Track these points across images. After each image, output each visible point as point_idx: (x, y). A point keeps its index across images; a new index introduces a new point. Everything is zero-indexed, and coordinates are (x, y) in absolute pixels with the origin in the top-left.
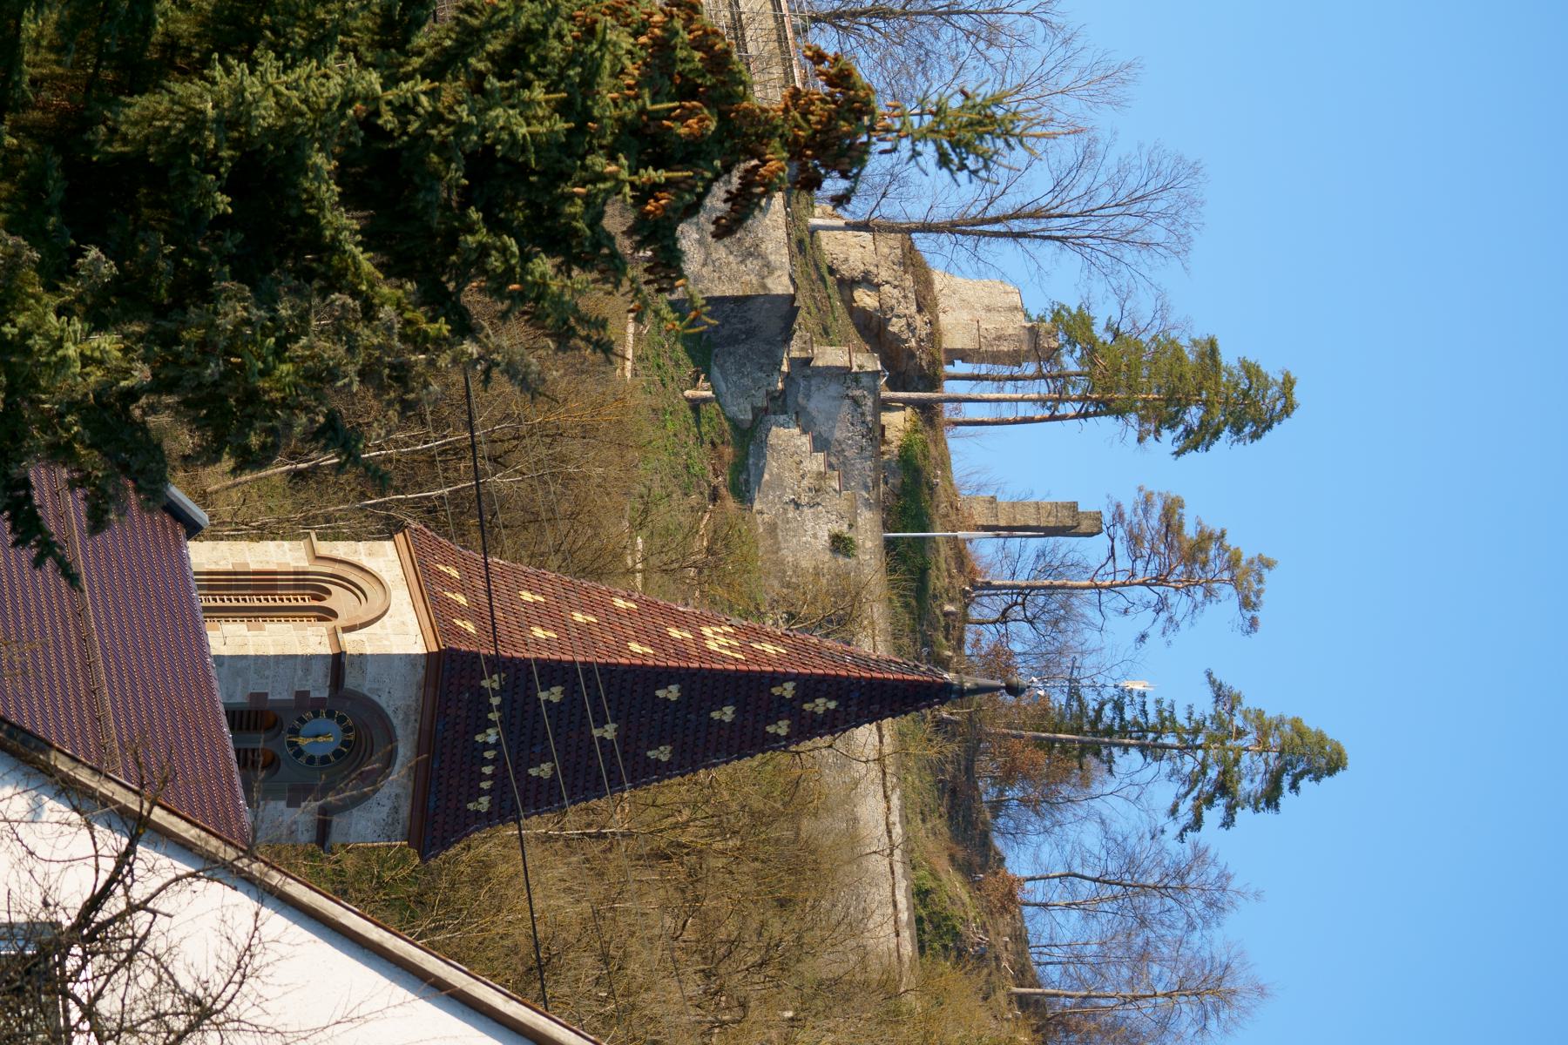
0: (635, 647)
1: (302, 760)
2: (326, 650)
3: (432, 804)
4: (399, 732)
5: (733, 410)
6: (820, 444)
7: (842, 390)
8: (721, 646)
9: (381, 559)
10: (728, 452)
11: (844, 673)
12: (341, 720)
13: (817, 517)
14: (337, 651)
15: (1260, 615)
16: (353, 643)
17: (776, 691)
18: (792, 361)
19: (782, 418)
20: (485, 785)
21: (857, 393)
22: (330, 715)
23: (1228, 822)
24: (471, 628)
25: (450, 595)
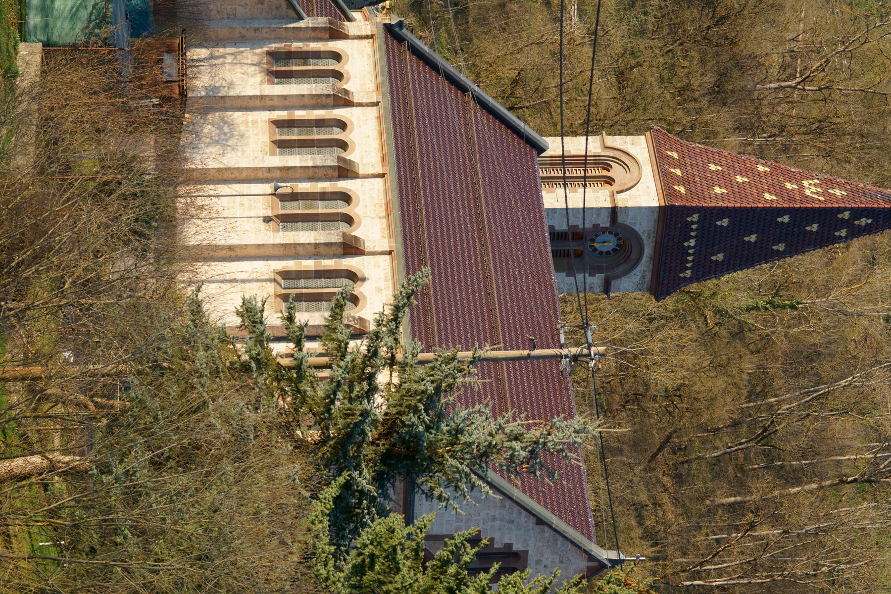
0: (767, 196)
1: (596, 253)
2: (608, 204)
3: (662, 276)
4: (645, 242)
8: (812, 193)
9: (638, 147)
11: (876, 206)
12: (616, 235)
14: (614, 206)
17: (840, 216)
22: (610, 233)
24: (682, 190)
25: (672, 170)
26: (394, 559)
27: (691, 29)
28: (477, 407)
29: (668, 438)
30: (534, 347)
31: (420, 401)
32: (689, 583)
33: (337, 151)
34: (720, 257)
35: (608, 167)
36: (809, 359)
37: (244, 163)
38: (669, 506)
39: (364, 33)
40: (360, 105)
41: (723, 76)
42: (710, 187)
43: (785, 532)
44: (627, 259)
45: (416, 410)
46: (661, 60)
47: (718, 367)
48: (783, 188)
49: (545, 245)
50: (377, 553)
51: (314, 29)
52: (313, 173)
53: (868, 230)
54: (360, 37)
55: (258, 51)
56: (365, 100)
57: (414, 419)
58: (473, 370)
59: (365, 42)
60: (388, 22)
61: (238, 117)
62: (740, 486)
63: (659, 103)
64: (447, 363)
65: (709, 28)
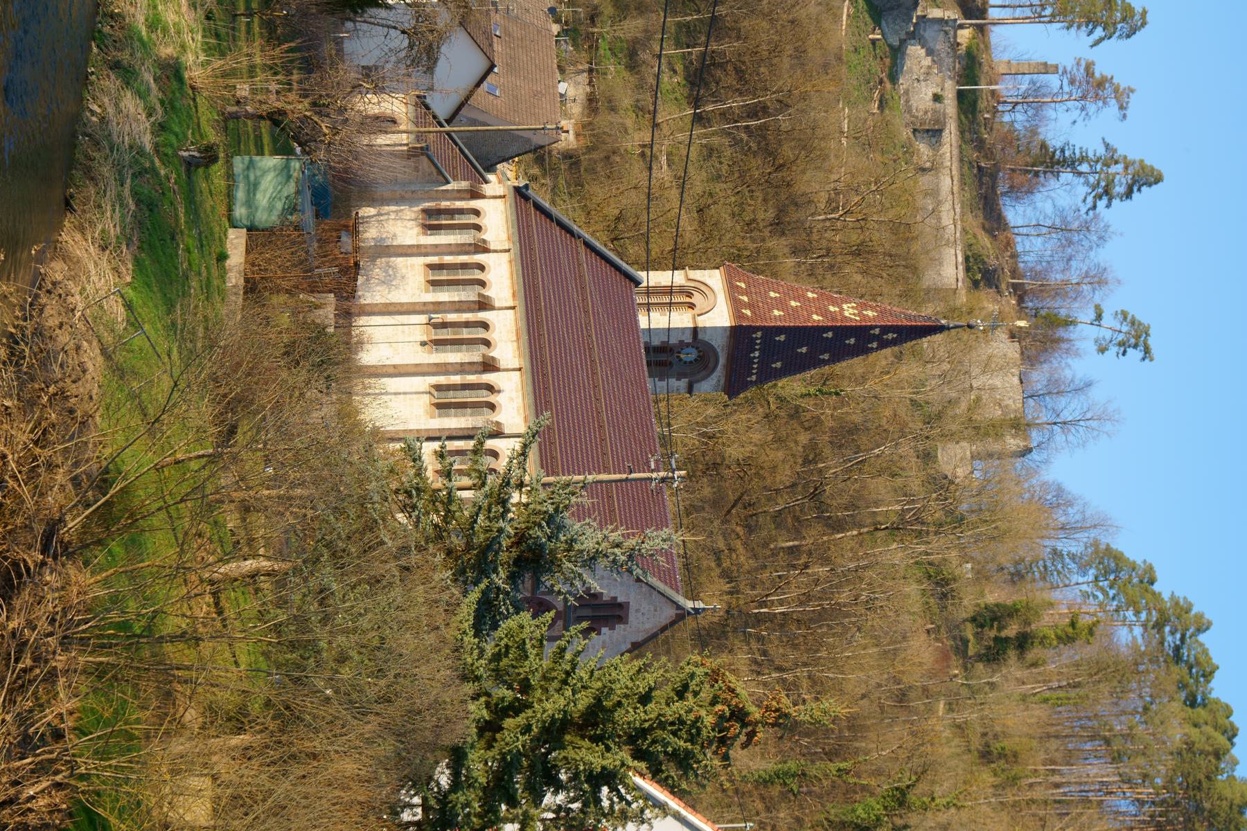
0: (815, 317)
2: (691, 325)
5: (890, 40)
6: (930, 52)
7: (940, 27)
10: (888, 61)
12: (697, 348)
13: (927, 86)
15: (1128, 112)
16: (704, 322)
17: (872, 332)
18: (918, 17)
19: (913, 41)
20: (754, 371)
21: (947, 28)
23: (1109, 206)
26: (524, 648)
27: (756, 174)
28: (587, 520)
29: (740, 498)
30: (631, 472)
31: (543, 519)
32: (756, 611)
33: (478, 288)
34: (779, 365)
35: (690, 295)
36: (850, 432)
37: (404, 299)
38: (741, 549)
39: (498, 194)
40: (495, 251)
41: (781, 211)
42: (770, 310)
43: (832, 570)
44: (706, 367)
45: (540, 526)
46: (733, 199)
47: (778, 440)
48: (827, 310)
49: (641, 358)
50: (510, 644)
51: (459, 191)
52: (459, 307)
53: (894, 343)
54: (495, 197)
55: (416, 209)
56: (499, 248)
57: (539, 533)
58: (584, 493)
59: (499, 201)
60: (516, 184)
61: (400, 261)
62: (797, 533)
63: (731, 235)
64: (563, 489)
65: (770, 173)
